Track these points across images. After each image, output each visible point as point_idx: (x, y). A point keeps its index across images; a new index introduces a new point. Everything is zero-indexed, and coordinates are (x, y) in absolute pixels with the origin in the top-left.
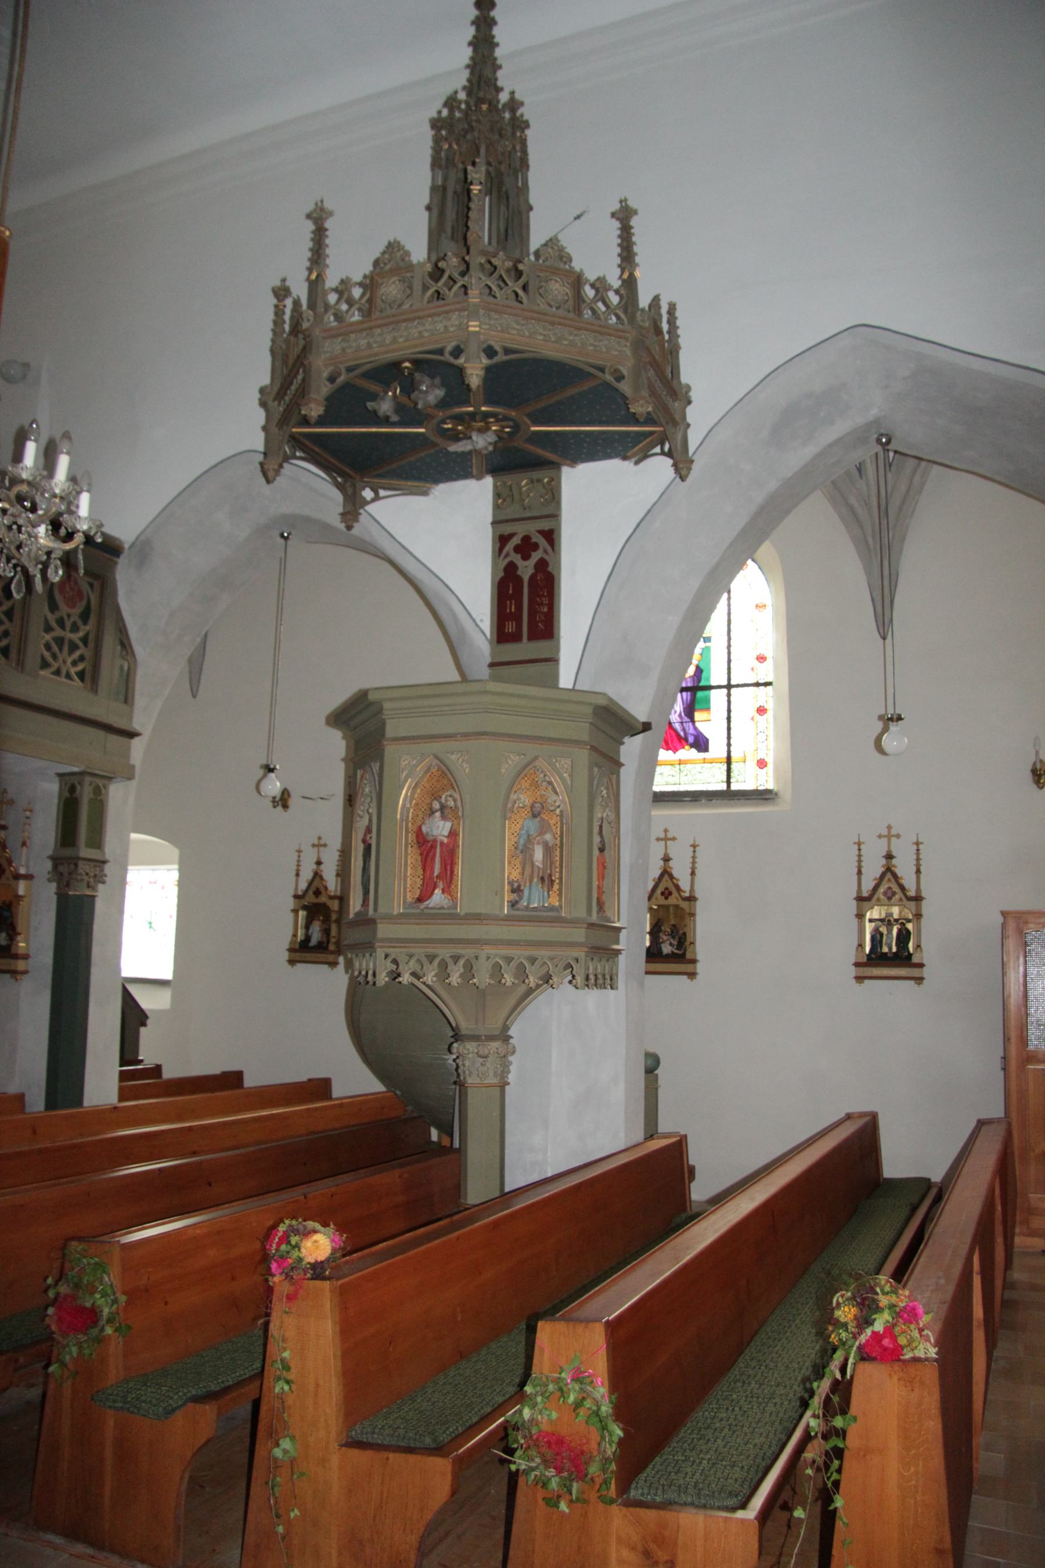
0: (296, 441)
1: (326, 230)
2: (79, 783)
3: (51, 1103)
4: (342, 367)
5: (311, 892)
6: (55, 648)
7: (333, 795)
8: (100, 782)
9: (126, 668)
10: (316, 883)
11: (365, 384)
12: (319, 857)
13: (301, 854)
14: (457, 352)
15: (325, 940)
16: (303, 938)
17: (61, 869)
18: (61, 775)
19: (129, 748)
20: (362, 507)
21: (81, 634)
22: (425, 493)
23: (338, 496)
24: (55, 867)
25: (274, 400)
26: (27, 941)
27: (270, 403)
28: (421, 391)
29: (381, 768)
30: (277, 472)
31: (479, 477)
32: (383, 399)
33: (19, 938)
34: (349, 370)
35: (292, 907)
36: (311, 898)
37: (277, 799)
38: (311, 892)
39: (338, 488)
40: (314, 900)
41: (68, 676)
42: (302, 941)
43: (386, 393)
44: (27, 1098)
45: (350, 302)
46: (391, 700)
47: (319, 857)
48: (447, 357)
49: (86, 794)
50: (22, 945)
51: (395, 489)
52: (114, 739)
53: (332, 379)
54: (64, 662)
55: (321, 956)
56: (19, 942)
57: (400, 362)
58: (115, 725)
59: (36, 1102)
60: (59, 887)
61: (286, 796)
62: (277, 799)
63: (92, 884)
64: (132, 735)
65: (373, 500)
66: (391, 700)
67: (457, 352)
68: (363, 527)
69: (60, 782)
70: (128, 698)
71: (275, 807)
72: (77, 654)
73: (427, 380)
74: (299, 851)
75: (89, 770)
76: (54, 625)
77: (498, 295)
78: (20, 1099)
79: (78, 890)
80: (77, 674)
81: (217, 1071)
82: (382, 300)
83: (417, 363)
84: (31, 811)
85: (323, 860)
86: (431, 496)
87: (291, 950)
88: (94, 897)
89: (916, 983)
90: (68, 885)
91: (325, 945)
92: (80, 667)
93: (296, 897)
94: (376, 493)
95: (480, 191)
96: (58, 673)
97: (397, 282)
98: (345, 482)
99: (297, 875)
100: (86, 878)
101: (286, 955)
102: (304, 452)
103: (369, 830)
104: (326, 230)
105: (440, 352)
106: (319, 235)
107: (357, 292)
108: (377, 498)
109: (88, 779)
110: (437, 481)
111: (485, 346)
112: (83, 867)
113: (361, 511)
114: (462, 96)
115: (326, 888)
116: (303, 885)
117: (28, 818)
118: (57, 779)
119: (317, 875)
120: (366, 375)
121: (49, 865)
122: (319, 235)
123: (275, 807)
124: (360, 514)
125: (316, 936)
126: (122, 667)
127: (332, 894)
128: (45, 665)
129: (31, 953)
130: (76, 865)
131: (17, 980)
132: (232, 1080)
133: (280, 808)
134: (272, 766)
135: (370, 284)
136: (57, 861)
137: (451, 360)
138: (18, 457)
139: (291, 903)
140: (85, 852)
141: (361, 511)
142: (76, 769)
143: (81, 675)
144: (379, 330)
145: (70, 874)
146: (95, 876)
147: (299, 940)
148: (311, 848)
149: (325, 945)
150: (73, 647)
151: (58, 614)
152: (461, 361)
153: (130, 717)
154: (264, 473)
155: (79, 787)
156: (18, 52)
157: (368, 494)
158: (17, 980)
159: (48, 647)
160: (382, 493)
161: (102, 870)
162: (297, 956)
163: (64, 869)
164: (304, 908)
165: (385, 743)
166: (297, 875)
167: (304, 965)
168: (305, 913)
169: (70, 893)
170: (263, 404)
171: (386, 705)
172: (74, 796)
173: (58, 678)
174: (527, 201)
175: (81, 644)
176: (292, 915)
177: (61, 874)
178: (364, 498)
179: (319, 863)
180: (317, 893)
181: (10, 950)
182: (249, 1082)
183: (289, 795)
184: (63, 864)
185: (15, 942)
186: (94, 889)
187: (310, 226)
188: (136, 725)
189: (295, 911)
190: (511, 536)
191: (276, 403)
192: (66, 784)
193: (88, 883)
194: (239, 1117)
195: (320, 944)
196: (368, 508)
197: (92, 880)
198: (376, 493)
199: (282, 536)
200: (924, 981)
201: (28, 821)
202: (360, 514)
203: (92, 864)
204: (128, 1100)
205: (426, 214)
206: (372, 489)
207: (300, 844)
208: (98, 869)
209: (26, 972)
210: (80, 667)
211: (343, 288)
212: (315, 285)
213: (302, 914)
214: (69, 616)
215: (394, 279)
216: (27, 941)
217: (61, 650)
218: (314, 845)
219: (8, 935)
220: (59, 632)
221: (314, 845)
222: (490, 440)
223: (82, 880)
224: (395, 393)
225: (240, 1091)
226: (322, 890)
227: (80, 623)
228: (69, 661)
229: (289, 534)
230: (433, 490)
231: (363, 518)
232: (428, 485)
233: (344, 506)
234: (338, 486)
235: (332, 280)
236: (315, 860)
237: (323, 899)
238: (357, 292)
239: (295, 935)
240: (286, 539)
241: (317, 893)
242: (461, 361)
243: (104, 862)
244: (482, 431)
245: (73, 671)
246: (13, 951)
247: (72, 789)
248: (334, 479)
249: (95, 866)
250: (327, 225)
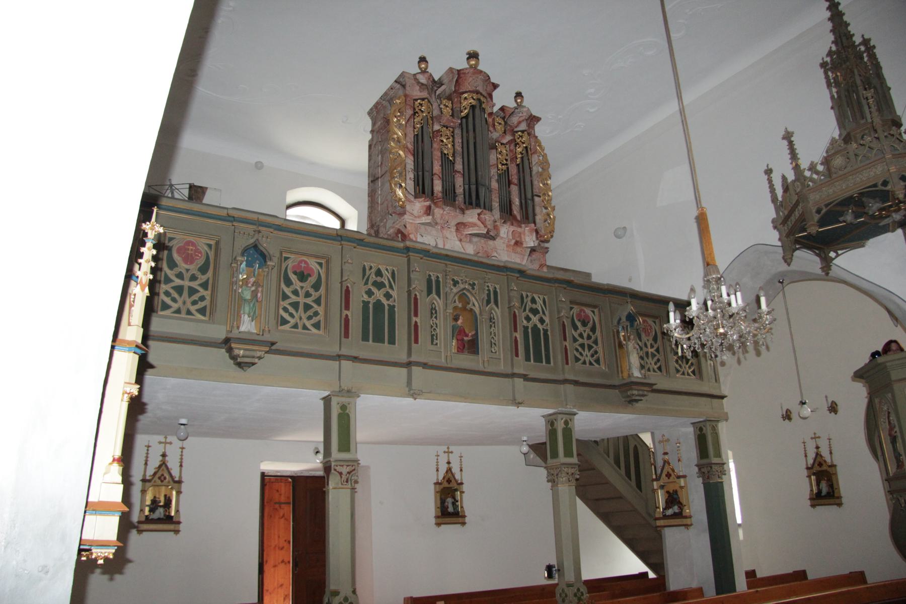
0: (797, 241)
1: (793, 141)
2: (704, 426)
3: (719, 589)
4: (822, 205)
5: (816, 465)
6: (580, 349)
7: (817, 408)
8: (714, 424)
9: (712, 365)
10: (819, 459)
11: (839, 208)
12: (817, 445)
13: (805, 444)
14: (885, 183)
15: (831, 491)
16: (817, 492)
17: (703, 470)
18: (692, 423)
19: (723, 404)
20: (831, 262)
21: (655, 348)
22: (863, 246)
23: (817, 259)
24: (700, 469)
25: (780, 225)
26: (689, 509)
27: (779, 227)
28: (869, 207)
29: (893, 396)
30: (791, 259)
31: (893, 231)
32: (847, 214)
33: (685, 508)
34: (827, 206)
35: (806, 475)
36: (817, 468)
37: (784, 416)
38: (816, 465)
39: (817, 256)
40: (819, 469)
41: (688, 375)
42: (816, 493)
43: (848, 211)
44: (703, 589)
45: (817, 173)
46: (889, 361)
47: (817, 445)
48: (880, 187)
49: (708, 431)
50: (687, 511)
51: (846, 248)
52: (715, 401)
53: (818, 211)
54: (184, 303)
55: (832, 501)
56: (686, 510)
57: (852, 196)
58: (715, 394)
59: (710, 592)
60: (703, 480)
61: (789, 413)
62: (784, 416)
63: (720, 476)
64: (722, 397)
65: (836, 257)
66: (889, 361)
67: (885, 183)
68: (834, 272)
69: (693, 427)
70: (717, 380)
71: (784, 420)
72: (655, 359)
73: (872, 201)
74: (804, 443)
75: (708, 419)
76: (578, 338)
77: (898, 148)
78: (700, 591)
79: (715, 480)
80: (692, 372)
81: (790, 571)
82: (835, 168)
83: (861, 194)
84: (680, 443)
85: (820, 446)
86: (867, 246)
87: (811, 499)
88: (722, 482)
89: (175, 533)
90: (708, 478)
91: (832, 494)
92: (658, 365)
93: (808, 468)
94: (837, 253)
95: (873, 101)
96: (683, 374)
97: (840, 157)
98: (820, 252)
99: (806, 456)
100: (717, 473)
101: (809, 502)
102: (799, 244)
103: (891, 428)
104: (793, 141)
105: (875, 185)
106: (791, 145)
107: (820, 168)
108: (838, 255)
109: (708, 424)
110: (868, 239)
111: (900, 176)
112: (715, 468)
113: (831, 264)
114: (834, 48)
115: (825, 461)
116: (811, 461)
117: (679, 447)
118: (692, 425)
119: (818, 455)
120: (837, 205)
121: (696, 469)
122: (791, 145)
123: (784, 420)
124: (831, 266)
125: (825, 490)
126: (710, 364)
127: (830, 464)
128: (678, 371)
129: (692, 515)
130: (711, 467)
131: (688, 529)
132: (801, 575)
133: (787, 420)
134: (804, 401)
135: (826, 161)
136: (700, 466)
137: (884, 188)
138: (759, 307)
139: (805, 473)
140: (715, 460)
141: (831, 264)
142: (701, 420)
143: (693, 372)
144: (838, 183)
145: (708, 472)
146: (721, 471)
147: (815, 493)
148: (811, 440)
149: (832, 494)
150: (590, 347)
151: (578, 331)
152: (889, 188)
153: (720, 387)
154: (786, 261)
155: (704, 428)
156: (687, 136)
157: (832, 254)
158: (688, 529)
159: (577, 350)
160: (840, 252)
161: (723, 468)
162: (816, 502)
163: (705, 470)
164: (814, 474)
165: (892, 383)
166: (806, 456)
167: (820, 507)
168: (815, 477)
169: (711, 482)
170: (775, 227)
171: (888, 364)
172: (554, 428)
173: (296, 330)
174: (886, 86)
175: (656, 353)
176: (807, 479)
177: (704, 473)
178: (831, 257)
179: (817, 448)
180: (820, 465)
181: (682, 514)
182: (811, 576)
183: (791, 413)
184: (703, 468)
185: (683, 510)
186: (722, 479)
187: (785, 143)
188: (725, 391)
189: (809, 477)
190: (293, 327)
191: (782, 225)
192: (697, 428)
193: (718, 475)
194: (791, 600)
195: (828, 493)
196: (834, 262)
197: (720, 474)
198: (837, 253)
199: (780, 282)
200: (180, 533)
201: (679, 449)
202: (831, 266)
203: (718, 466)
204: (723, 593)
205: (832, 111)
206: (834, 252)
207: (804, 439)
208: (721, 468)
209: (691, 525)
210: (658, 365)
211: (812, 167)
212: (797, 168)
213: (813, 477)
214: (585, 331)
215: (838, 156)
216: (689, 509)
217: (584, 350)
218: (812, 438)
219: (679, 507)
220: (581, 341)
221: (812, 438)
222: (902, 214)
223: (715, 474)
224: (852, 209)
225: (806, 581)
226: (823, 463)
227: (591, 334)
228: (653, 363)
229: (783, 281)
230: (867, 244)
231: (833, 268)
232: (864, 242)
233: (822, 264)
234: (817, 255)
235: (804, 164)
236: (815, 446)
237: (824, 468)
238: (820, 168)
239: (812, 490)
240: (782, 283)
241: (820, 465)
242: (889, 188)
243: (724, 464)
244: (896, 211)
245: (690, 371)
246: (684, 514)
247: (701, 429)
248: (815, 253)
249: (720, 466)
250: (792, 139)
